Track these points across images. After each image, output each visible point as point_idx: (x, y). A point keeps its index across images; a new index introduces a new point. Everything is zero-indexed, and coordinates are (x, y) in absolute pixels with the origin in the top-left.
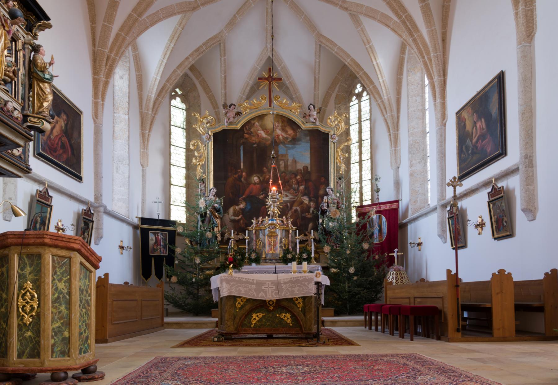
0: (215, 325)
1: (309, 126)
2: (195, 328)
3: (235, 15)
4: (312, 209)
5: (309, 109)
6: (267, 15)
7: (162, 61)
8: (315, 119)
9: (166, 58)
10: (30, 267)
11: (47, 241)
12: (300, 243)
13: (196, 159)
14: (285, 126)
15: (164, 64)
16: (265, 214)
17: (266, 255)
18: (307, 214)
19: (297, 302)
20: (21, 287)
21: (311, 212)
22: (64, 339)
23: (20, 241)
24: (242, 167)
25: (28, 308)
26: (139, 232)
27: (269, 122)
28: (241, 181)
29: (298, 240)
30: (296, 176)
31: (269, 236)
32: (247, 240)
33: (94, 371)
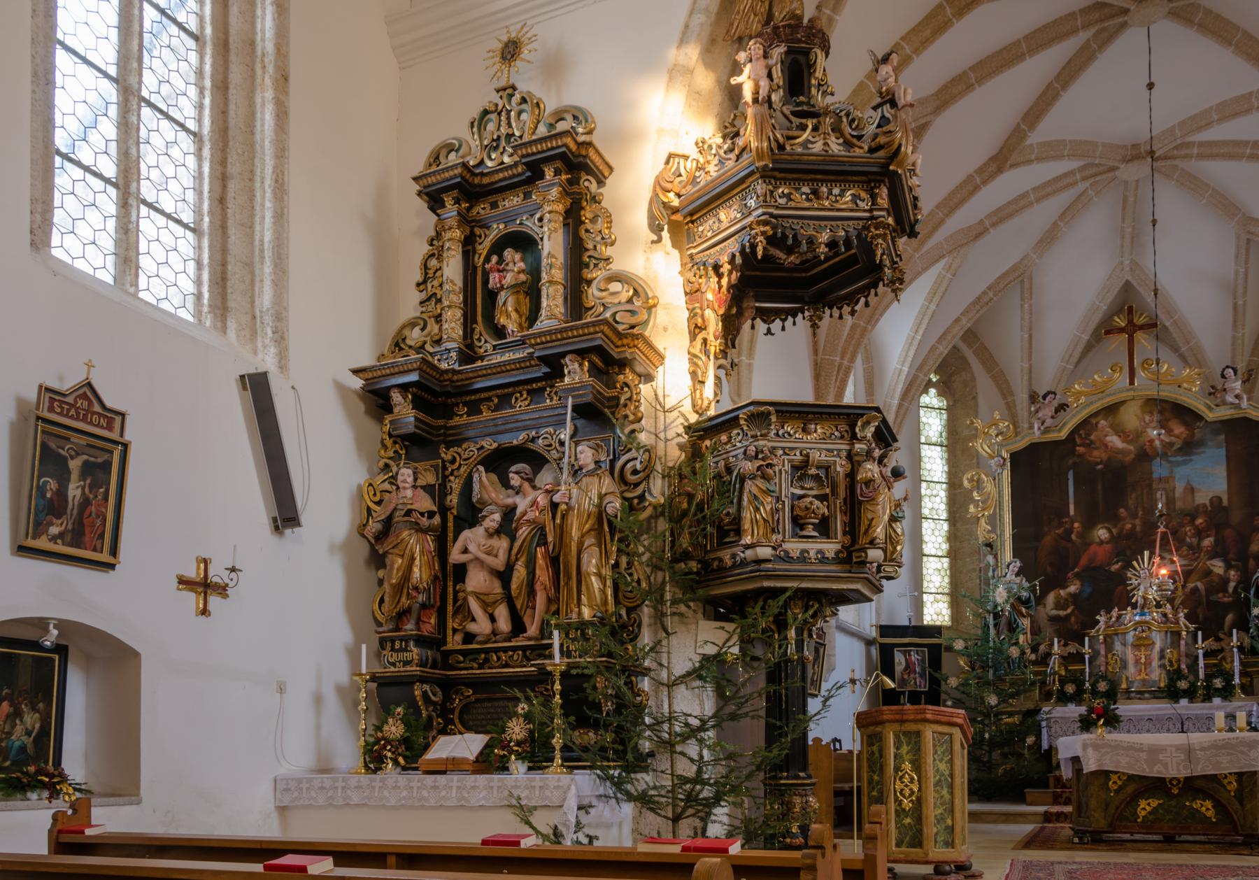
0: (1041, 818)
1: (1224, 413)
2: (1003, 822)
3: (1055, 223)
4: (1232, 585)
5: (1223, 376)
6: (1124, 208)
7: (913, 338)
8: (1237, 397)
9: (921, 332)
10: (908, 744)
11: (929, 716)
12: (1206, 655)
13: (977, 506)
14: (1168, 420)
15: (916, 343)
16: (1126, 601)
17: (1130, 683)
18: (1220, 595)
19: (1225, 782)
20: (897, 769)
21: (1231, 590)
22: (947, 828)
23: (898, 717)
24: (1072, 512)
25: (907, 792)
26: (874, 651)
27: (1131, 417)
28: (1070, 540)
29: (1201, 652)
30: (1194, 519)
31: (1136, 646)
32: (1087, 657)
33: (969, 868)
